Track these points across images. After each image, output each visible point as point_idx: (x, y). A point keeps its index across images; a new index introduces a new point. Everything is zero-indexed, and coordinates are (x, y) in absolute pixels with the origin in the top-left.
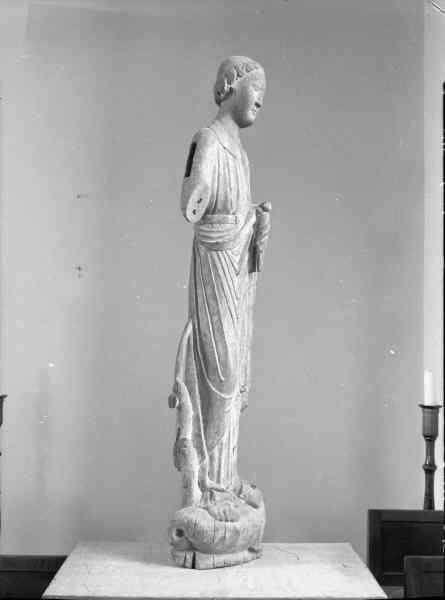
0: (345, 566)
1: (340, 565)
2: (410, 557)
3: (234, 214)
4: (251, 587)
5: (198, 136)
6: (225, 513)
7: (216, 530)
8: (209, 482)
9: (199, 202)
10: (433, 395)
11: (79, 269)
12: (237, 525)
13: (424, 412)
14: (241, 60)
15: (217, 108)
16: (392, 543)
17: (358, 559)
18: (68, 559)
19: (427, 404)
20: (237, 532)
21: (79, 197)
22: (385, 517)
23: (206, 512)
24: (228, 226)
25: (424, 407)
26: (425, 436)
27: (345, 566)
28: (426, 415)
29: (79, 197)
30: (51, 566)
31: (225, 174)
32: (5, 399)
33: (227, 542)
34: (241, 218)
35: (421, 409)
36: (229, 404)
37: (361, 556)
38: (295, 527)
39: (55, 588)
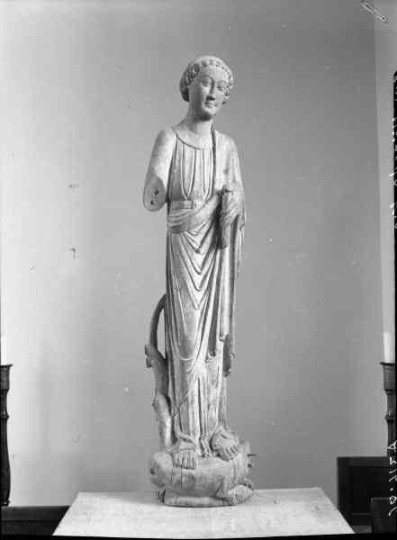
0: (318, 509)
1: (313, 508)
2: (375, 499)
3: (189, 199)
4: (233, 529)
5: (162, 132)
6: (183, 459)
7: (173, 474)
8: (179, 434)
9: (157, 193)
10: (389, 356)
11: (74, 250)
12: (193, 472)
13: (385, 369)
14: (207, 59)
15: (187, 103)
16: (357, 486)
17: (329, 502)
18: (70, 508)
19: (386, 362)
20: (192, 478)
21: (71, 186)
22: (352, 464)
23: (170, 457)
24: (185, 211)
25: (384, 364)
26: (386, 390)
27: (318, 509)
28: (387, 371)
29: (71, 186)
30: (58, 513)
31: (180, 166)
32: (12, 368)
33: (185, 486)
34: (199, 203)
35: (382, 366)
36: (189, 366)
37: (331, 500)
38: (272, 474)
39: (60, 531)
